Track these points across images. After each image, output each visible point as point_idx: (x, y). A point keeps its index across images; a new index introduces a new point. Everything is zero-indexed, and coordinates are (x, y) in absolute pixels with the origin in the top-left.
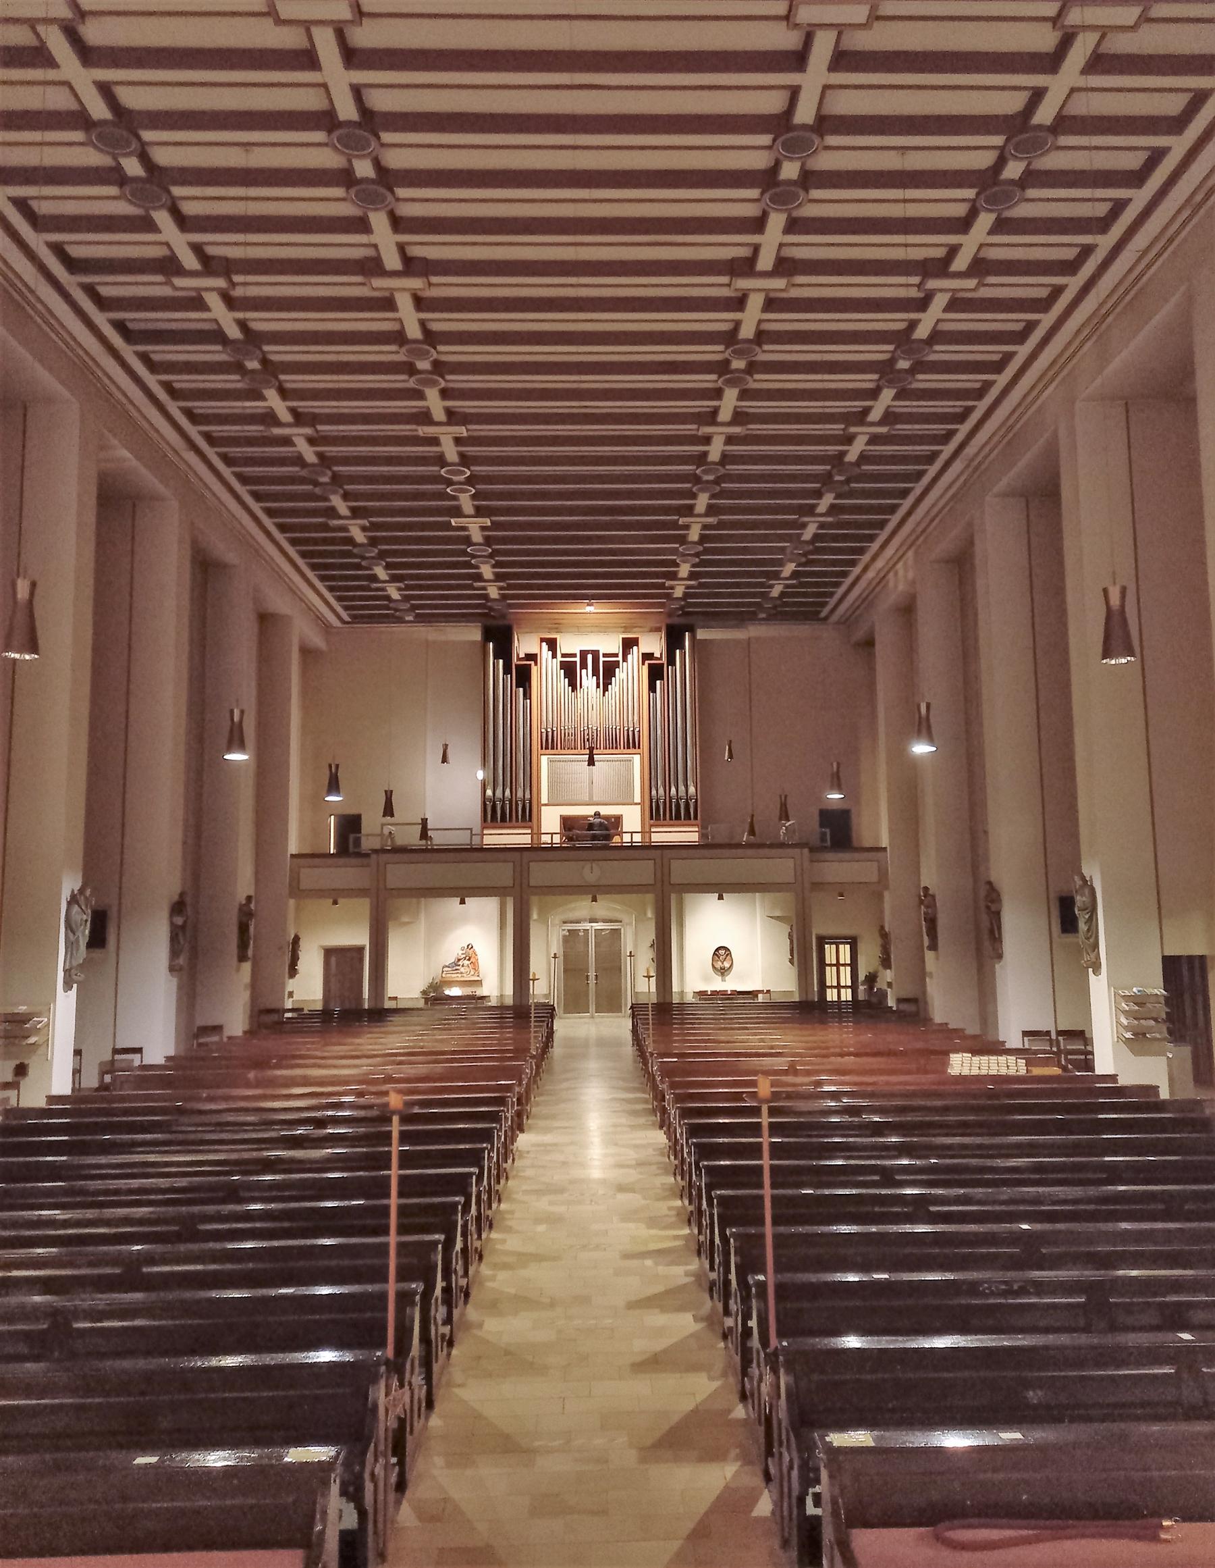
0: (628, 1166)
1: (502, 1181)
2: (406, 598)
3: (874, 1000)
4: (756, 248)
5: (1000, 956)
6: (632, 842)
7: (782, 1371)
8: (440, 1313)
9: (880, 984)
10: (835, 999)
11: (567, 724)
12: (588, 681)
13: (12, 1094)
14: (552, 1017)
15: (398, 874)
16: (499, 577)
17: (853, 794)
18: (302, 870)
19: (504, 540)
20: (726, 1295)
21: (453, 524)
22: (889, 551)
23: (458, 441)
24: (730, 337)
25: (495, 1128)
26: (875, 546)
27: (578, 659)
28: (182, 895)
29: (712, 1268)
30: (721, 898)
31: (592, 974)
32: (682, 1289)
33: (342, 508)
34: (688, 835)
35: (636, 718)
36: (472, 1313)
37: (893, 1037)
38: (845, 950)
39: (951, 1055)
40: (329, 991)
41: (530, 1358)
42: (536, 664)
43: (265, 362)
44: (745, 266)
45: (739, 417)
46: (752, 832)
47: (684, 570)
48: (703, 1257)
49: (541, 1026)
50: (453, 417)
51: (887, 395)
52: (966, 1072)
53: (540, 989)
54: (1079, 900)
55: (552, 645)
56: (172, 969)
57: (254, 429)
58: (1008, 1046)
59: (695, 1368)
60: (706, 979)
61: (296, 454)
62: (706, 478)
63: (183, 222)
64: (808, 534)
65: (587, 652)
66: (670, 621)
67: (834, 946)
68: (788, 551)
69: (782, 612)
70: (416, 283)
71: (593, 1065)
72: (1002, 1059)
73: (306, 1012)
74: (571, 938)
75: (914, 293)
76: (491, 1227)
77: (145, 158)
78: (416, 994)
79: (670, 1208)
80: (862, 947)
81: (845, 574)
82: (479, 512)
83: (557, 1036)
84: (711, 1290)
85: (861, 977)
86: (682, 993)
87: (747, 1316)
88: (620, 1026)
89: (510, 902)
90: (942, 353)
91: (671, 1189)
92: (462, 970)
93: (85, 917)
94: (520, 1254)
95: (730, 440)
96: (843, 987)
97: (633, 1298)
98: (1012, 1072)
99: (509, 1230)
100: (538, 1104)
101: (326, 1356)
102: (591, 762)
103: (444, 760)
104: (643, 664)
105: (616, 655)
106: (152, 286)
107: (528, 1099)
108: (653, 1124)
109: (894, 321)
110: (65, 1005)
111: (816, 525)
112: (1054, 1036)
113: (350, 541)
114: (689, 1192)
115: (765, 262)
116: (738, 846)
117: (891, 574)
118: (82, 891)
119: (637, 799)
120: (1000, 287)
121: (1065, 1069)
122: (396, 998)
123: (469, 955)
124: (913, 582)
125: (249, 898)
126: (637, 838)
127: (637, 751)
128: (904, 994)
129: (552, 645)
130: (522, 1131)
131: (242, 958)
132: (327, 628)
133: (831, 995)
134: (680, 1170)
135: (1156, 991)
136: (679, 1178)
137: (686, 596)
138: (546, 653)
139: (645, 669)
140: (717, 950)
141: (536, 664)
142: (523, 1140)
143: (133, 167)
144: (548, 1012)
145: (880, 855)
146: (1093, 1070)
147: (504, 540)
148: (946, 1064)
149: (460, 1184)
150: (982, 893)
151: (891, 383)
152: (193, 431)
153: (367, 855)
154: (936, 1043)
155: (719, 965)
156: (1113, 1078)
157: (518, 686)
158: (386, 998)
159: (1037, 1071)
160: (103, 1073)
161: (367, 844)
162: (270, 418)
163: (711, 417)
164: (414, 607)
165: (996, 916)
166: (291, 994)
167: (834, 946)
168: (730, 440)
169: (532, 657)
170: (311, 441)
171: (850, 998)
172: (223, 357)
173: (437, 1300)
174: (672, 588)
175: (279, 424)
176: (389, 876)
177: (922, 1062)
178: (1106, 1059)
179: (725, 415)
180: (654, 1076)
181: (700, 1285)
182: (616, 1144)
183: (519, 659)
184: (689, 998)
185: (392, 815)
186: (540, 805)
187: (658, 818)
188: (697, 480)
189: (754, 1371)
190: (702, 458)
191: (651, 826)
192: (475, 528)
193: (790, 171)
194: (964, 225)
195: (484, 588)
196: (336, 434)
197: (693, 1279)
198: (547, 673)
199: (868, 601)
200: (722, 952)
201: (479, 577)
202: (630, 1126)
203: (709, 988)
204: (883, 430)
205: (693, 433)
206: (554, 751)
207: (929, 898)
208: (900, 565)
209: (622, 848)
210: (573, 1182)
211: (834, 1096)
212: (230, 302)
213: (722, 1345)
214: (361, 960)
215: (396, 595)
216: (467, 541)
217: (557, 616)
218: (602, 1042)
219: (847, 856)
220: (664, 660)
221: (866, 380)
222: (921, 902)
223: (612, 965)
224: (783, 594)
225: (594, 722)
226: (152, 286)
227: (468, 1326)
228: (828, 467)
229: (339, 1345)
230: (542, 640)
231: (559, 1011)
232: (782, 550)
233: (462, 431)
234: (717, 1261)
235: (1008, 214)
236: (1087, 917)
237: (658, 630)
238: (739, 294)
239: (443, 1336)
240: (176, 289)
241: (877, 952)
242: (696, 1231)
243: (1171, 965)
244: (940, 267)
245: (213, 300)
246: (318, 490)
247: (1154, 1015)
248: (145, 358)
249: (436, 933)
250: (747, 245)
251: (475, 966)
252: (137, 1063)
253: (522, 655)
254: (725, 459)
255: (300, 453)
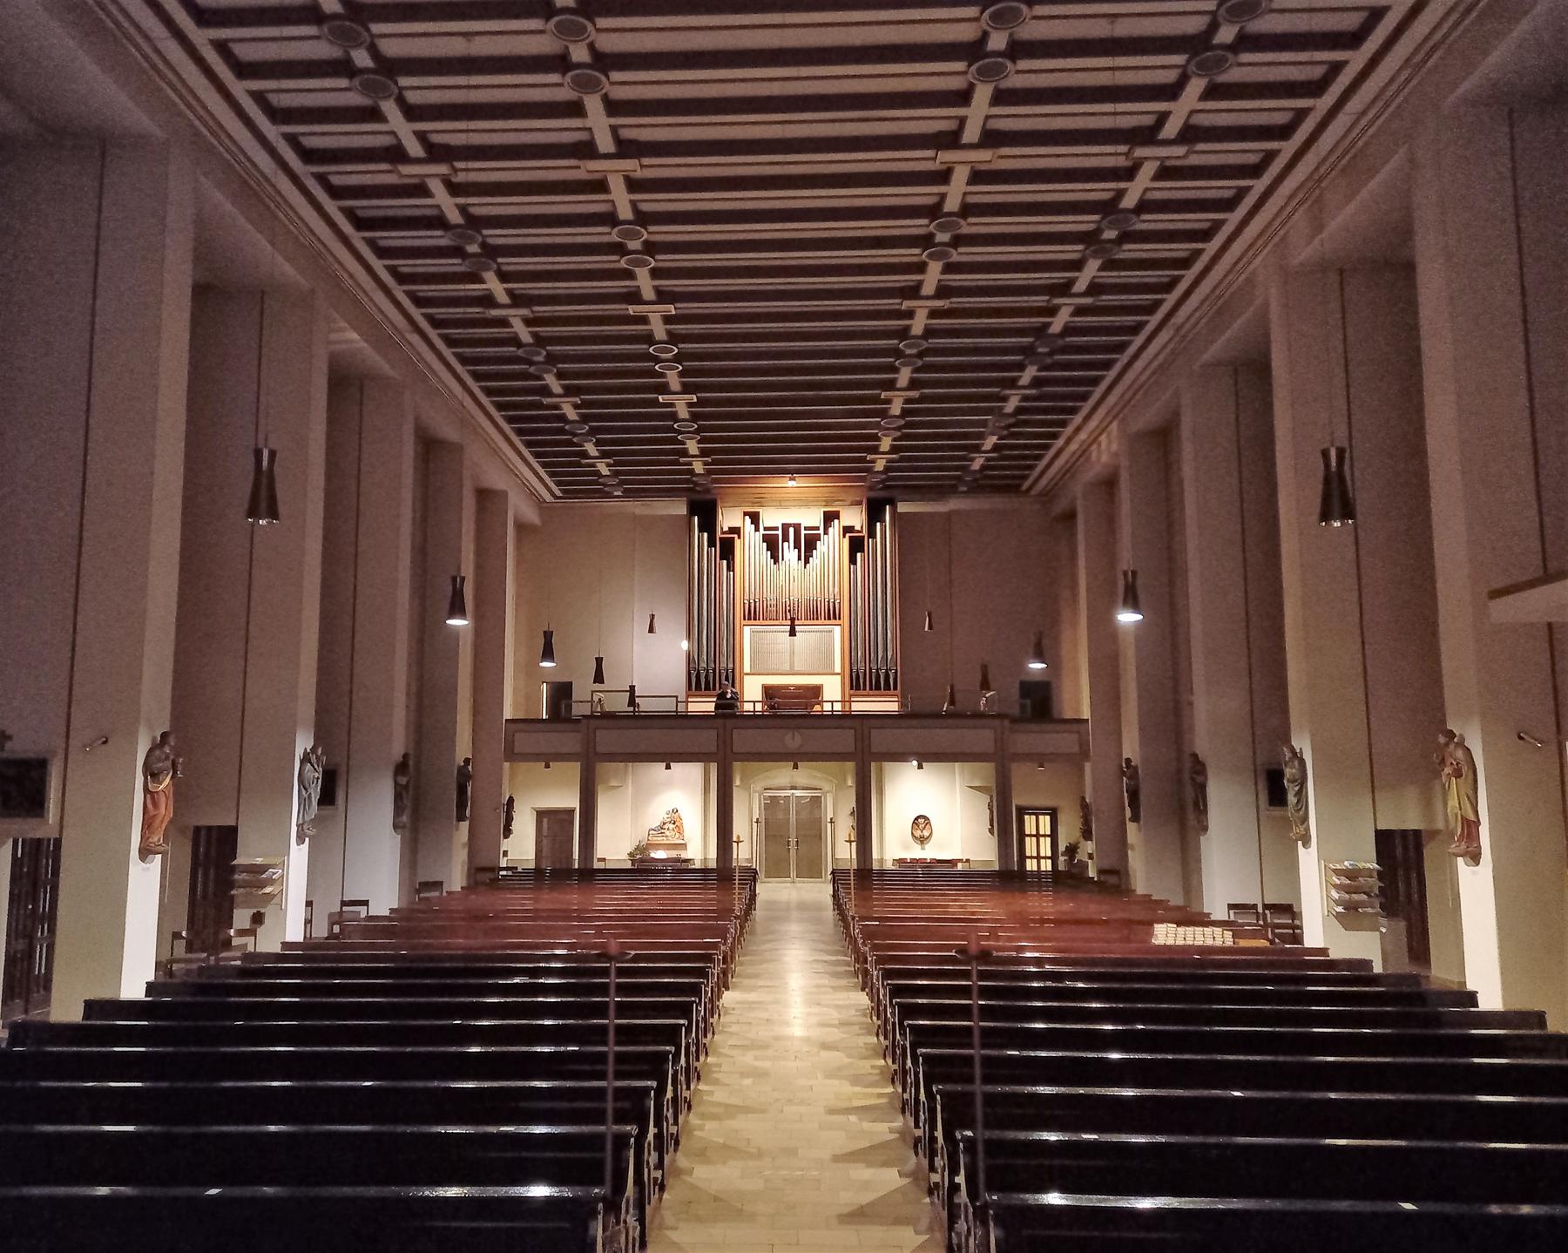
0: (833, 1026)
1: (709, 1036)
2: (616, 474)
3: (1075, 871)
4: (962, 121)
5: (1205, 829)
6: (832, 711)
7: (991, 1224)
8: (653, 1158)
9: (1081, 856)
10: (1035, 869)
11: (770, 596)
12: (790, 553)
13: (250, 940)
14: (755, 880)
15: (607, 739)
16: (704, 453)
17: (1054, 665)
18: (517, 735)
19: (909, 449)
20: (932, 1154)
21: (661, 400)
22: (1093, 424)
23: (668, 320)
24: (933, 211)
25: (703, 983)
26: (1078, 419)
27: (780, 532)
28: (405, 756)
29: (917, 1126)
30: (920, 767)
31: (793, 841)
32: (884, 1146)
33: (556, 386)
34: (888, 705)
35: (837, 590)
36: (681, 1160)
37: (1092, 907)
38: (1045, 822)
39: (1156, 926)
40: (541, 851)
41: (739, 1205)
42: (739, 538)
43: (484, 245)
44: (951, 140)
45: (943, 291)
46: (952, 702)
47: (886, 444)
48: (908, 1114)
49: (743, 889)
50: (663, 297)
51: (1092, 268)
52: (1170, 942)
53: (743, 853)
54: (1288, 772)
55: (755, 518)
56: (395, 827)
57: (474, 311)
58: (1213, 918)
59: (899, 1221)
60: (906, 847)
61: (512, 335)
62: (908, 352)
63: (412, 112)
64: (1010, 406)
65: (790, 525)
66: (872, 494)
67: (1034, 817)
68: (990, 424)
69: (984, 484)
70: (629, 165)
71: (794, 928)
72: (1208, 930)
73: (519, 870)
74: (772, 805)
75: (1121, 162)
76: (699, 1078)
77: (374, 51)
78: (625, 857)
79: (873, 1067)
80: (1061, 818)
81: (1047, 447)
82: (687, 389)
83: (758, 899)
84: (915, 1147)
85: (1062, 848)
86: (881, 861)
87: (954, 1171)
88: (822, 891)
89: (714, 767)
90: (1151, 222)
91: (874, 1050)
92: (667, 833)
93: (316, 775)
94: (727, 1106)
95: (933, 314)
96: (1034, 858)
97: (838, 1152)
98: (1218, 943)
99: (716, 1082)
100: (742, 964)
101: (540, 1191)
102: (793, 633)
103: (651, 630)
104: (844, 537)
105: (818, 528)
106: (379, 174)
107: (732, 958)
108: (855, 986)
109: (1099, 191)
110: (299, 856)
111: (1018, 398)
112: (1260, 910)
113: (562, 418)
114: (892, 1051)
115: (971, 134)
116: (937, 715)
117: (1094, 447)
118: (314, 749)
119: (838, 669)
120: (1207, 154)
121: (1272, 942)
122: (604, 860)
123: (674, 819)
124: (1116, 455)
125: (467, 761)
126: (838, 707)
127: (837, 622)
128: (1106, 865)
129: (755, 518)
130: (727, 989)
131: (461, 818)
132: (540, 502)
133: (1031, 865)
134: (883, 1031)
135: (1368, 865)
136: (882, 1038)
137: (887, 469)
138: (749, 527)
139: (846, 542)
140: (917, 819)
141: (739, 538)
142: (728, 998)
143: (362, 58)
144: (751, 876)
145: (1082, 727)
146: (1302, 943)
147: (909, 449)
148: (1151, 934)
149: (671, 1035)
150: (1188, 765)
151: (1095, 254)
152: (416, 313)
153: (578, 721)
154: (1138, 914)
155: (918, 833)
156: (1323, 951)
157: (721, 559)
158: (595, 860)
159: (1243, 943)
160: (332, 924)
161: (579, 710)
162: (488, 300)
163: (913, 292)
164: (623, 482)
165: (1201, 789)
166: (505, 853)
167: (1034, 817)
168: (933, 314)
169: (736, 531)
170: (528, 322)
171: (1050, 868)
172: (444, 242)
173: (649, 1144)
174: (873, 461)
175: (496, 305)
176: (851, 740)
177: (1126, 932)
178: (1316, 932)
179: (929, 288)
180: (856, 939)
181: (904, 1141)
182: (819, 1004)
183: (723, 533)
184: (889, 865)
185: (603, 682)
186: (742, 674)
187: (858, 688)
188: (898, 353)
189: (961, 1226)
190: (903, 333)
191: (851, 696)
192: (682, 406)
193: (998, 41)
194: (1171, 92)
195: (690, 464)
196: (550, 314)
197: (897, 1135)
198: (750, 546)
199: (1069, 471)
200: (920, 820)
201: (685, 453)
202: (832, 987)
203: (908, 856)
204: (1088, 301)
205: (897, 307)
206: (757, 622)
207: (1131, 770)
208: (1103, 438)
209: (822, 717)
210: (777, 1038)
211: (1038, 962)
212: (454, 189)
213: (928, 1200)
214: (572, 823)
215: (605, 471)
216: (674, 417)
217: (764, 491)
218: (803, 906)
219: (1050, 727)
220: (865, 533)
221: (1072, 251)
222: (1124, 773)
223: (813, 831)
224: (984, 468)
225: (795, 596)
226: (379, 174)
227: (678, 1172)
228: (1031, 340)
229: (551, 1181)
230: (745, 514)
231: (761, 875)
232: (984, 424)
233: (671, 309)
234: (922, 1117)
235: (1223, 78)
236: (1297, 788)
237: (859, 503)
238: (944, 167)
239: (656, 1179)
240: (402, 176)
241: (1077, 824)
242: (900, 1090)
243: (1384, 839)
244: (1147, 135)
245: (436, 187)
246: (532, 369)
247: (1367, 890)
248: (371, 243)
249: (643, 797)
250: (955, 117)
251: (680, 829)
252: (363, 915)
253: (726, 529)
254: (929, 333)
255: (516, 333)
